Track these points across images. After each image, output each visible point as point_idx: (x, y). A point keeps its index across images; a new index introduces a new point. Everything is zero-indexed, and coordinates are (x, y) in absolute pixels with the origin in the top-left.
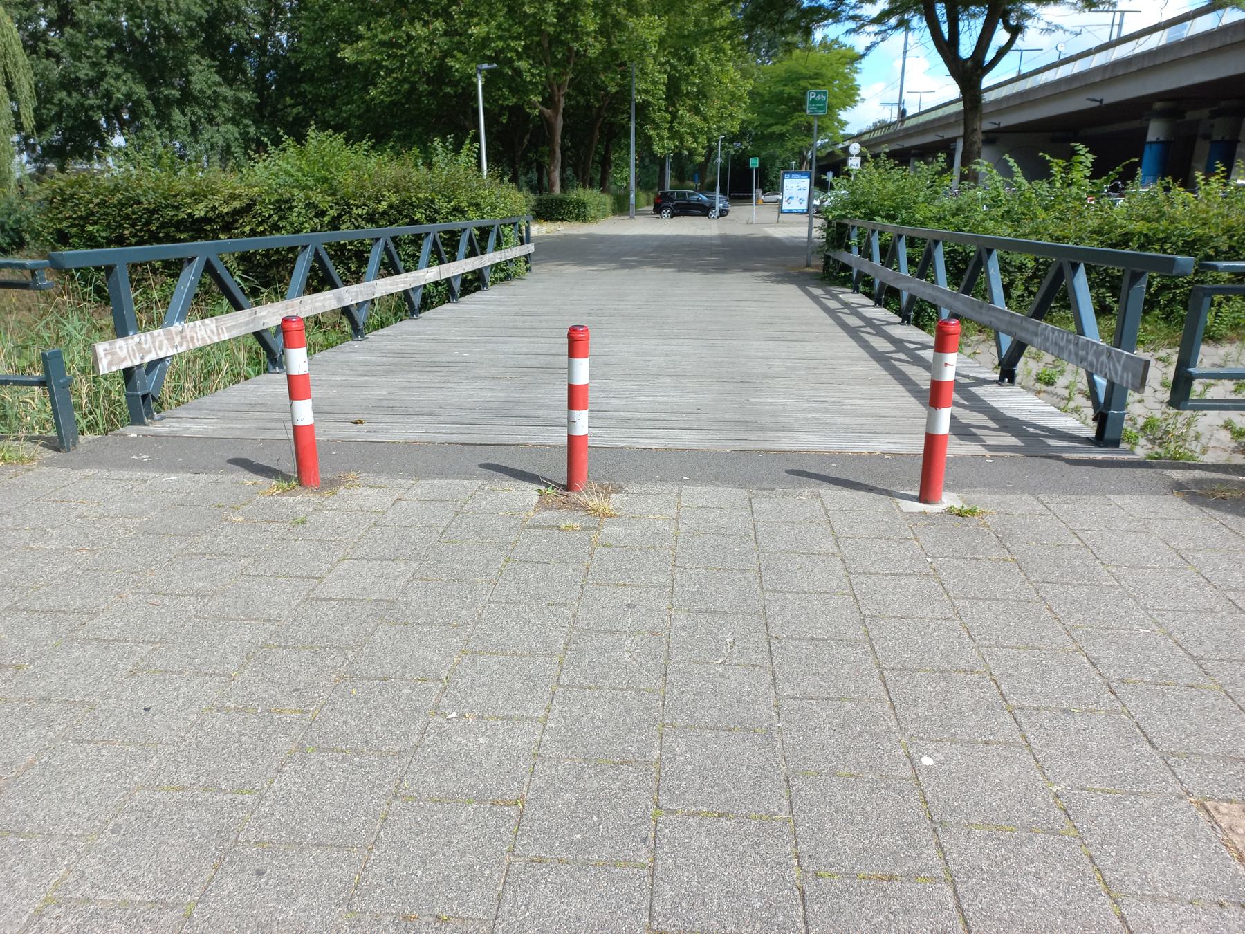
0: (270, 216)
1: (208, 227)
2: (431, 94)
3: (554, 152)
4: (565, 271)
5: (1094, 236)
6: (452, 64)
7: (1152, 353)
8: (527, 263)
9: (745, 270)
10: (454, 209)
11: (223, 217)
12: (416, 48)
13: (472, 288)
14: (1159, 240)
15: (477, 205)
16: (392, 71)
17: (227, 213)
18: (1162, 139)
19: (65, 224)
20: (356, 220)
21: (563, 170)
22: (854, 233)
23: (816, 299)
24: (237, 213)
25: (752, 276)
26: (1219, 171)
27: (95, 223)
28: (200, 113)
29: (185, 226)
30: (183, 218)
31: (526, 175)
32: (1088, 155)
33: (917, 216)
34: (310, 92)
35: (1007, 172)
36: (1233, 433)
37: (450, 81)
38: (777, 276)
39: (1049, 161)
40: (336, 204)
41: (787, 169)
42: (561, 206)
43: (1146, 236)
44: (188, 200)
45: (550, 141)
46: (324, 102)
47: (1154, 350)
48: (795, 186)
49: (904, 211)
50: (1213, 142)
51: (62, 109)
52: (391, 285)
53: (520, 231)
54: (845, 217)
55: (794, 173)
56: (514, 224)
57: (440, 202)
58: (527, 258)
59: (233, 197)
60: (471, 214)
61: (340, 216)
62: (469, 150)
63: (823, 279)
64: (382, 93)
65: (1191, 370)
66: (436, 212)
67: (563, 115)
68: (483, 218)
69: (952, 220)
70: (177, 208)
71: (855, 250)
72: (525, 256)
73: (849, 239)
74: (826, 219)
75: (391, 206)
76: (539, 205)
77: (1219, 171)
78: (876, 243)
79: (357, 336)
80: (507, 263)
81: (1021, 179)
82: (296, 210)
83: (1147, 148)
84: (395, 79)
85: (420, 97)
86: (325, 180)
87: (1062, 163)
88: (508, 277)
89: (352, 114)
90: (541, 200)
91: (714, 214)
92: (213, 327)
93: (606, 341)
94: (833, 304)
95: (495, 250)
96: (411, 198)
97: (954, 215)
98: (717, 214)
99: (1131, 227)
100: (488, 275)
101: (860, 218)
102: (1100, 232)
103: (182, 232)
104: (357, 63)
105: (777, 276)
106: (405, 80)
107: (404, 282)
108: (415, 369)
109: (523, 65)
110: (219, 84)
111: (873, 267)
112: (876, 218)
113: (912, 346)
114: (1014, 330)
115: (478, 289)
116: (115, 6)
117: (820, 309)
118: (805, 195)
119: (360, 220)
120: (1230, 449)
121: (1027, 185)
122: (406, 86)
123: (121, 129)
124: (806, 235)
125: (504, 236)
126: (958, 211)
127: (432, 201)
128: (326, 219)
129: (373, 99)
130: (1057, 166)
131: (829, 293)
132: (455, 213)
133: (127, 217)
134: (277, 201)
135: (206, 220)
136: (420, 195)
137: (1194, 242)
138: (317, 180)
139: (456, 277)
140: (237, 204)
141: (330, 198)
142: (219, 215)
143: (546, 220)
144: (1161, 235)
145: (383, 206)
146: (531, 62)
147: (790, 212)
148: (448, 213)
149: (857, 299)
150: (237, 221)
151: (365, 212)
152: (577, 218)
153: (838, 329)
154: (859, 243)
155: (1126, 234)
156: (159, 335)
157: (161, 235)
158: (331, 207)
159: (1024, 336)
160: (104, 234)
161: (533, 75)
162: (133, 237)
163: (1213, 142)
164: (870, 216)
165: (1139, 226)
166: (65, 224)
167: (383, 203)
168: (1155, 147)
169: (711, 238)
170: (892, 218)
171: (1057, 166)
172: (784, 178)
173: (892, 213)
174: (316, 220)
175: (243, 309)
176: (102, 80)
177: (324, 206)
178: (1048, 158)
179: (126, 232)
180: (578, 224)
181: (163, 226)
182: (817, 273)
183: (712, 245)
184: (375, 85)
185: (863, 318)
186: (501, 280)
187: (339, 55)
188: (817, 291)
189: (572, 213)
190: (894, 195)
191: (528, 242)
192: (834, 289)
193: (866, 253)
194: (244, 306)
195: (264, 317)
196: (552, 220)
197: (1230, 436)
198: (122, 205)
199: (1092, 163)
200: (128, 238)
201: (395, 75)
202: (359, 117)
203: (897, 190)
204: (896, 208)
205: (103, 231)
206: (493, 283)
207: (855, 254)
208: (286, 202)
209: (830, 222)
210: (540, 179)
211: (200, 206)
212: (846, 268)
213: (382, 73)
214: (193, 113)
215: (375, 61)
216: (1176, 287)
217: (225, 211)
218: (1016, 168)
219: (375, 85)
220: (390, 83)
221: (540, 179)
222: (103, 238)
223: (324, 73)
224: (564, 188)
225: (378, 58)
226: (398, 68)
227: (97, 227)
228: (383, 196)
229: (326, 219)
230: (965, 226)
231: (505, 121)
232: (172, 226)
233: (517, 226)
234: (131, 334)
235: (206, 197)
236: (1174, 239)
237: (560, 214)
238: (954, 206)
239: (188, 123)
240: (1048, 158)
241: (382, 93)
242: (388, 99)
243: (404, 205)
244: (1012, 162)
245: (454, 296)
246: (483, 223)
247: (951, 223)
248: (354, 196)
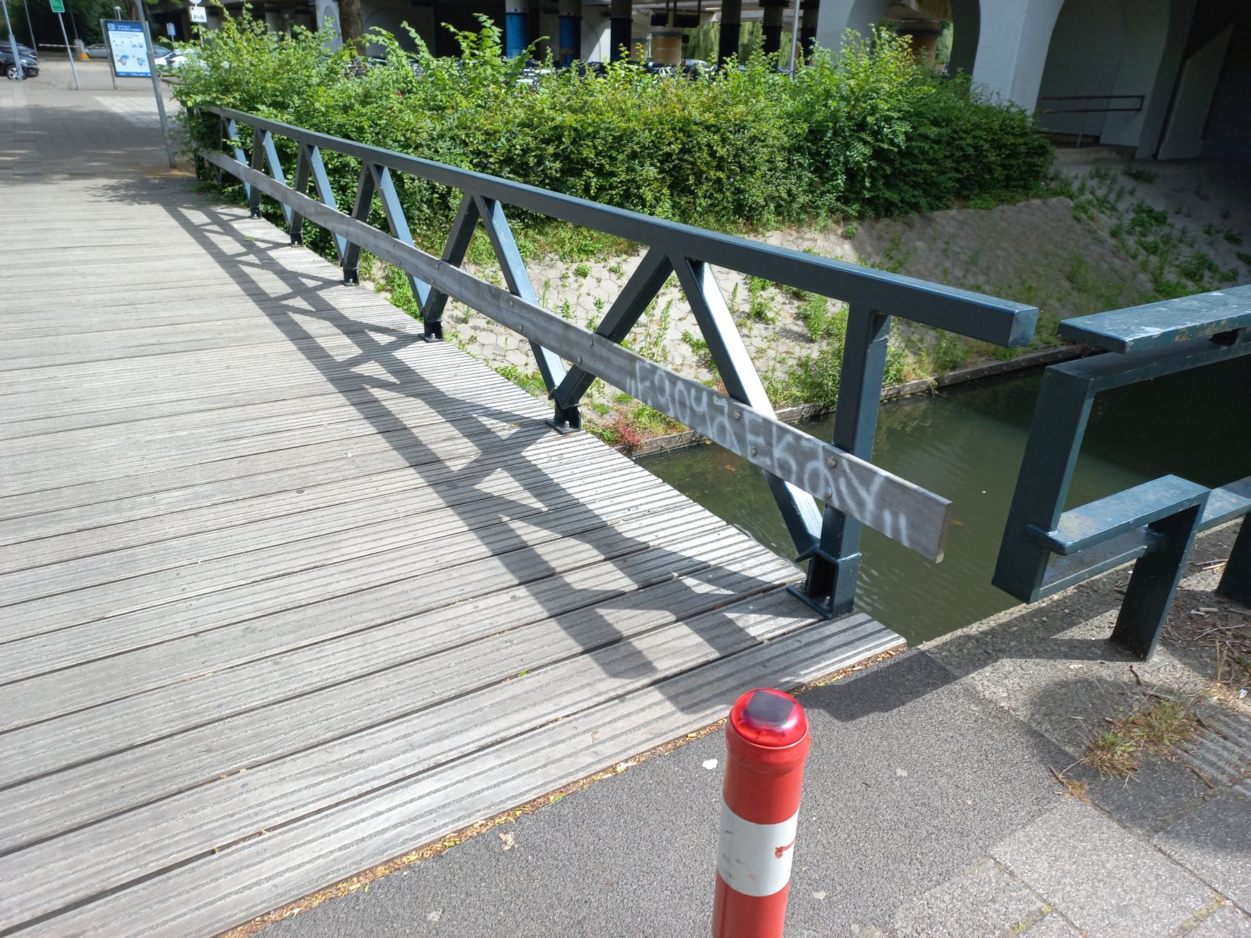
5: (526, 130)
7: (603, 264)
9: (74, 175)
14: (589, 135)
18: (519, 11)
22: (233, 128)
23: (196, 232)
25: (87, 189)
26: (623, 55)
32: (494, 28)
33: (317, 105)
35: (409, 46)
36: (692, 346)
38: (128, 187)
39: (456, 34)
41: (110, 16)
43: (576, 130)
47: (605, 260)
48: (127, 41)
49: (296, 98)
50: (561, 17)
54: (212, 103)
55: (120, 23)
63: (201, 190)
65: (1051, 534)
69: (364, 111)
71: (240, 154)
73: (227, 136)
74: (183, 103)
77: (623, 55)
78: (269, 144)
81: (425, 53)
83: (508, 18)
87: (472, 36)
91: (16, 72)
94: (229, 246)
97: (364, 103)
98: (21, 73)
99: (559, 119)
101: (234, 107)
102: (530, 125)
105: (128, 187)
111: (277, 186)
112: (259, 106)
113: (383, 339)
114: (576, 353)
116: (1077, 194)
117: (210, 258)
118: (142, 53)
120: (694, 364)
121: (435, 62)
124: (156, 110)
126: (366, 99)
130: (465, 41)
131: (216, 219)
137: (621, 137)
144: (590, 130)
147: (129, 75)
149: (261, 230)
153: (251, 305)
154: (243, 144)
155: (556, 128)
159: (590, 364)
163: (561, 17)
164: (250, 102)
165: (569, 119)
168: (514, 18)
169: (14, 112)
170: (281, 106)
171: (465, 41)
172: (107, 30)
173: (280, 99)
178: (452, 29)
182: (189, 179)
183: (16, 125)
185: (283, 274)
188: (197, 217)
190: (276, 73)
192: (223, 211)
193: (257, 159)
197: (690, 349)
199: (499, 37)
203: (280, 67)
204: (284, 93)
207: (241, 161)
209: (190, 110)
212: (230, 179)
216: (611, 188)
218: (419, 41)
230: (380, 118)
236: (602, 133)
238: (360, 90)
240: (452, 29)
244: (413, 33)
247: (362, 115)
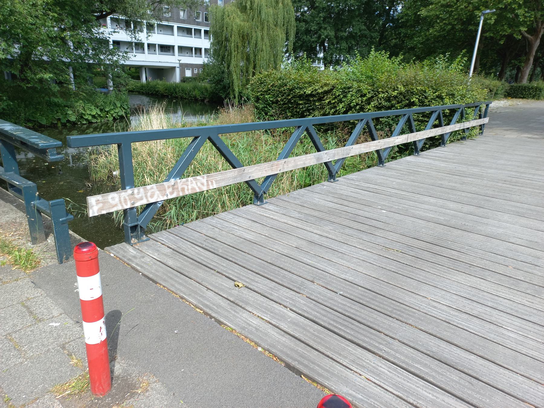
0: (339, 95)
1: (311, 99)
2: (462, 30)
3: (529, 60)
4: (506, 136)
6: (478, 13)
8: (481, 129)
10: (437, 97)
11: (320, 94)
12: (460, 6)
13: (437, 143)
15: (453, 95)
16: (444, 20)
17: (321, 93)
19: (259, 94)
20: (381, 100)
21: (534, 69)
24: (326, 93)
27: (269, 94)
28: (353, 43)
29: (303, 98)
30: (302, 94)
31: (511, 71)
34: (403, 32)
37: (474, 23)
40: (372, 90)
42: (525, 90)
44: (307, 85)
45: (528, 54)
46: (408, 37)
51: (304, 43)
52: (364, 148)
53: (480, 111)
56: (476, 107)
57: (430, 93)
58: (481, 127)
59: (326, 85)
60: (446, 100)
61: (372, 97)
62: (460, 62)
64: (436, 31)
66: (426, 98)
67: (541, 39)
68: (454, 103)
70: (301, 89)
72: (481, 126)
75: (401, 93)
76: (510, 89)
79: (331, 179)
80: (464, 131)
82: (351, 93)
84: (445, 24)
85: (455, 32)
86: (371, 78)
88: (463, 138)
89: (419, 42)
90: (512, 86)
92: (204, 181)
93: (506, 217)
95: (458, 122)
96: (413, 89)
100: (446, 138)
103: (301, 100)
104: (427, 17)
106: (450, 24)
107: (377, 146)
108: (338, 220)
109: (520, 12)
110: (365, 30)
115: (439, 145)
119: (382, 100)
122: (449, 27)
123: (324, 52)
125: (467, 114)
127: (425, 92)
128: (365, 98)
129: (431, 34)
132: (437, 99)
133: (281, 92)
134: (345, 88)
135: (311, 95)
136: (418, 88)
138: (367, 77)
139: (420, 141)
140: (326, 89)
141: (370, 88)
142: (318, 93)
143: (512, 98)
145: (395, 93)
146: (526, 10)
148: (432, 99)
150: (324, 97)
151: (385, 95)
152: (533, 97)
156: (152, 188)
157: (292, 101)
158: (369, 93)
160: (271, 99)
161: (526, 17)
162: (282, 101)
166: (259, 94)
167: (396, 92)
174: (360, 99)
175: (236, 168)
176: (319, 30)
177: (365, 91)
179: (279, 99)
180: (533, 100)
181: (294, 97)
184: (433, 27)
186: (459, 140)
187: (418, 13)
189: (530, 94)
191: (485, 117)
194: (237, 167)
195: (252, 173)
196: (516, 97)
198: (281, 86)
200: (280, 102)
201: (445, 22)
202: (422, 44)
205: (272, 97)
206: (452, 142)
208: (349, 88)
210: (517, 75)
211: (310, 88)
213: (438, 21)
214: (351, 43)
215: (437, 15)
217: (320, 91)
219: (433, 27)
220: (441, 26)
221: (517, 75)
222: (271, 101)
223: (412, 23)
224: (530, 80)
225: (438, 13)
226: (447, 18)
227: (269, 96)
228: (398, 88)
229: (365, 98)
231: (502, 43)
232: (298, 97)
233: (478, 108)
234: (127, 188)
235: (314, 84)
237: (522, 94)
239: (347, 47)
241: (436, 31)
242: (438, 34)
243: (408, 93)
245: (417, 151)
246: (453, 106)
248: (382, 87)
